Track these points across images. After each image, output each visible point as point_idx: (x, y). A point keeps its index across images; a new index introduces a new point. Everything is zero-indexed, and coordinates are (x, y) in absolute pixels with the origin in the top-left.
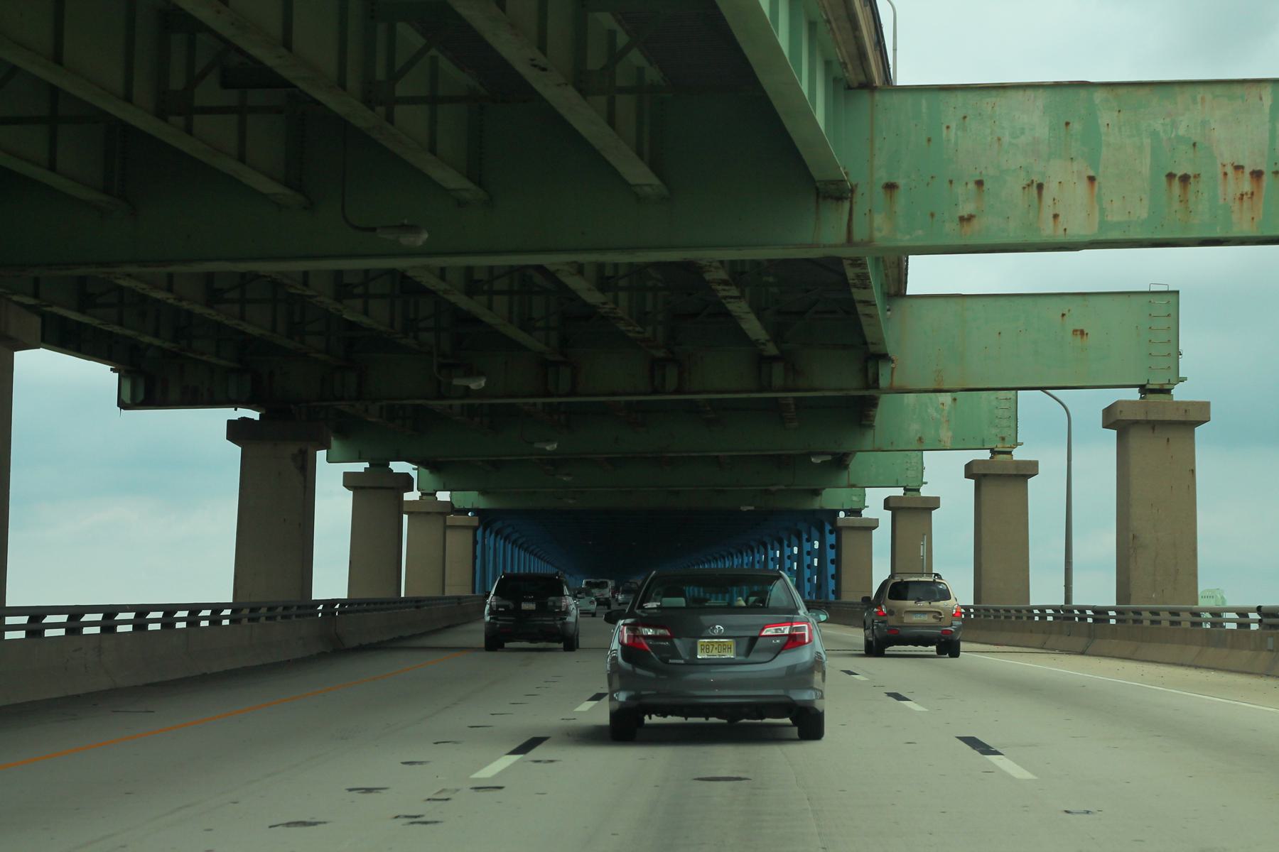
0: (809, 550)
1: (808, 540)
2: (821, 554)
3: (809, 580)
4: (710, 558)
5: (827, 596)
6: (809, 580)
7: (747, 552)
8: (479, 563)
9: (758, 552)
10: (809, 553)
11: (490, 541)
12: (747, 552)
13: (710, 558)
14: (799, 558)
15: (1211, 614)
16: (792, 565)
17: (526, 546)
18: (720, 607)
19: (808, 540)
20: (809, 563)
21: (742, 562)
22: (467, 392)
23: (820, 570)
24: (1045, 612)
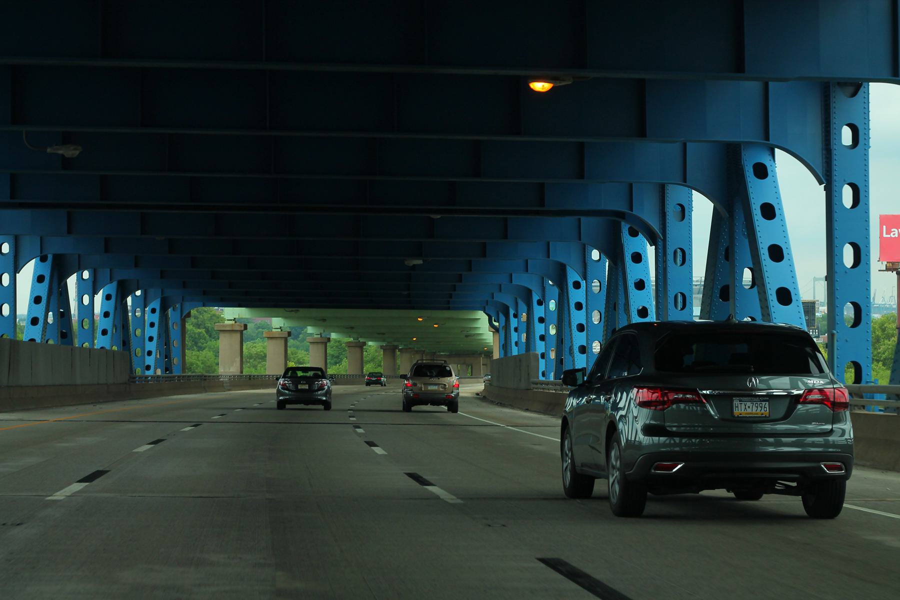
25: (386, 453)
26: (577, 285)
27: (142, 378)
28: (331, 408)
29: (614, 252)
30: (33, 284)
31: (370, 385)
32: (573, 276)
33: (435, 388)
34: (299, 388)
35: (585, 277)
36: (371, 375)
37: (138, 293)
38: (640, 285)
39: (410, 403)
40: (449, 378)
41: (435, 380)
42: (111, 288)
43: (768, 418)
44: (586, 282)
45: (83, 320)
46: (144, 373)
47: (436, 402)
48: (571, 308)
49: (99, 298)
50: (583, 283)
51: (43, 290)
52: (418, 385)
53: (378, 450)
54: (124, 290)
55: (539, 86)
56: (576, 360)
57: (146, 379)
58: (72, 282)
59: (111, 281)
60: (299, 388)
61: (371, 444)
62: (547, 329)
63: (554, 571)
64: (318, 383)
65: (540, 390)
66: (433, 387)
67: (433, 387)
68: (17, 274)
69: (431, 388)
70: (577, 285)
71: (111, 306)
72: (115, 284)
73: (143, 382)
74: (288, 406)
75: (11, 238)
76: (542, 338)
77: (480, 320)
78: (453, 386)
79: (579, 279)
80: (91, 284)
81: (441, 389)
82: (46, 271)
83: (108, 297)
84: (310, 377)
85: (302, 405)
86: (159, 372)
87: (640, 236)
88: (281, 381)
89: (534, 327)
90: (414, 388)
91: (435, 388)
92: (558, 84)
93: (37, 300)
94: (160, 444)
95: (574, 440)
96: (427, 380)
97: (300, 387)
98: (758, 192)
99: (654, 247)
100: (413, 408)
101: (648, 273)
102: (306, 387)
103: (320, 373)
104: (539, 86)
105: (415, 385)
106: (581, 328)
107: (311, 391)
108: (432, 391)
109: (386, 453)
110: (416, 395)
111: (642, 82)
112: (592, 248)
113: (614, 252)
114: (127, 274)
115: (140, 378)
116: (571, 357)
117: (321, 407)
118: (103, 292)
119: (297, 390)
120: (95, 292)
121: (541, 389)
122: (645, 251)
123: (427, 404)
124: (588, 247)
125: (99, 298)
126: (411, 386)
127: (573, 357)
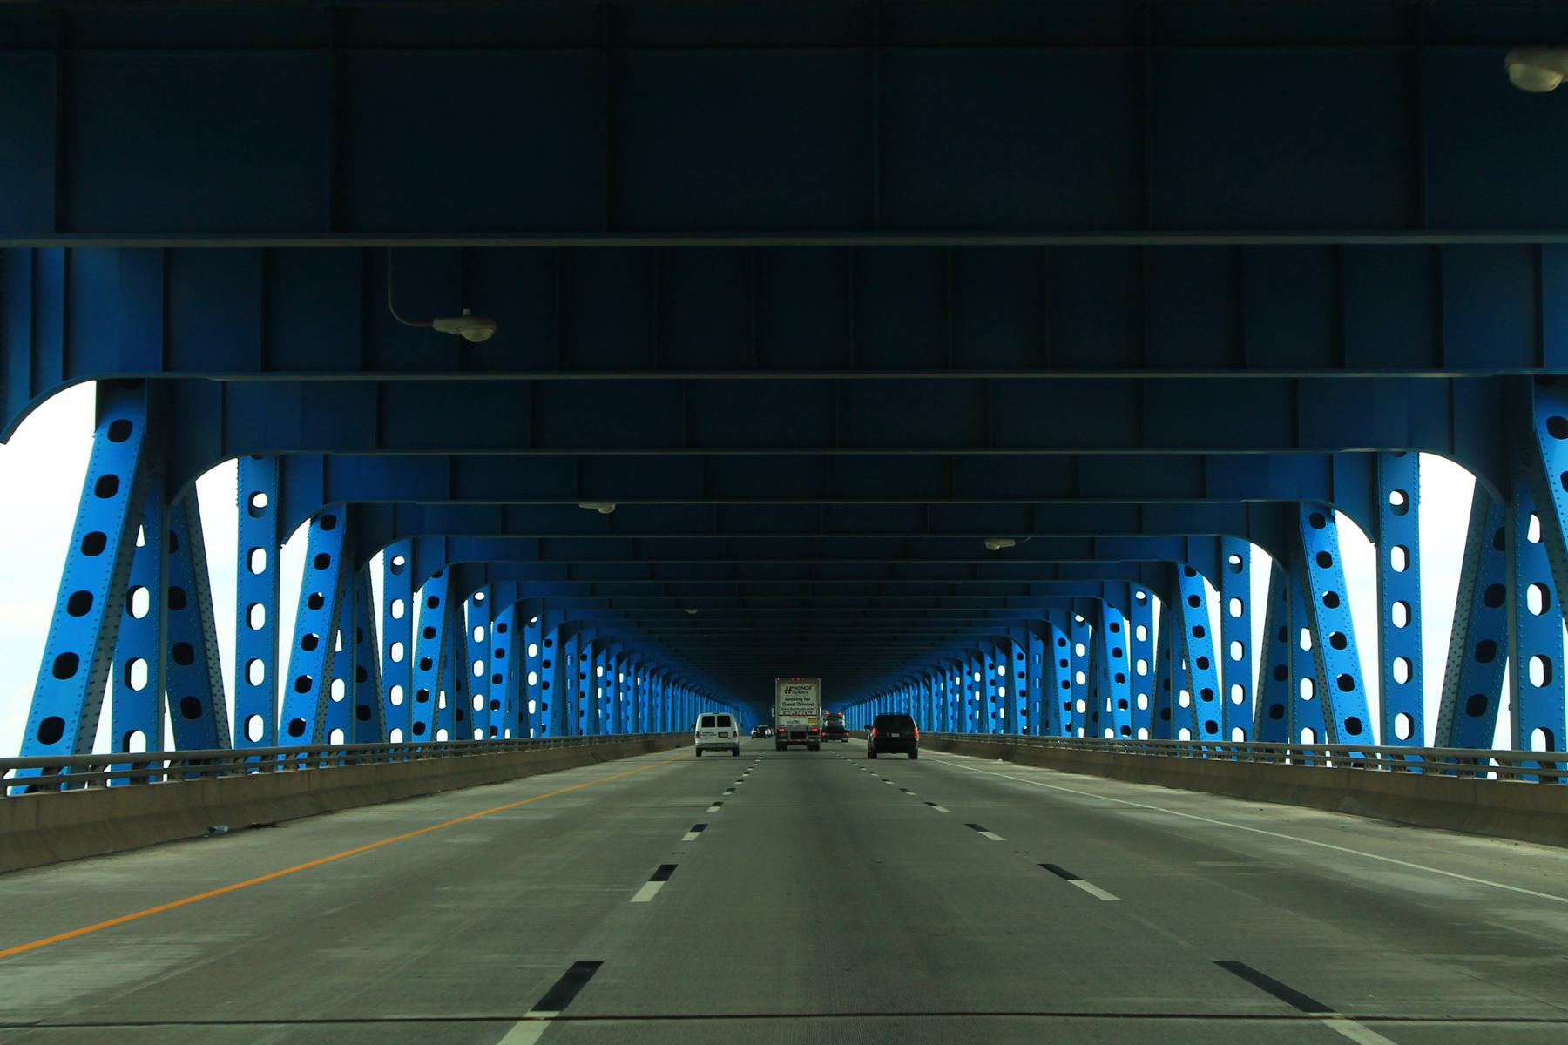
0: (970, 683)
1: (992, 667)
2: (1008, 681)
3: (994, 716)
4: (908, 680)
5: (1016, 732)
6: (971, 717)
7: (952, 672)
8: (859, 744)
9: (936, 683)
10: (992, 683)
11: (686, 695)
12: (913, 686)
13: (908, 680)
14: (982, 686)
15: (1222, 748)
16: (973, 696)
17: (701, 691)
18: (638, 699)
19: (992, 667)
20: (970, 698)
21: (919, 693)
22: (688, 615)
23: (1008, 702)
24: (1348, 755)
26: (1062, 643)
31: (826, 741)
32: (1059, 634)
35: (1069, 636)
37: (480, 596)
38: (1118, 653)
46: (540, 736)
50: (1068, 642)
54: (458, 593)
57: (413, 751)
58: (377, 564)
59: (486, 583)
62: (997, 691)
70: (1062, 643)
71: (437, 618)
73: (303, 767)
74: (789, 747)
76: (993, 699)
77: (602, 966)
79: (1063, 636)
82: (332, 544)
83: (432, 602)
87: (1198, 574)
89: (148, 979)
93: (314, 602)
95: (907, 762)
98: (1315, 542)
100: (879, 755)
106: (1066, 684)
111: (1536, 248)
115: (396, 750)
118: (424, 592)
122: (1123, 624)
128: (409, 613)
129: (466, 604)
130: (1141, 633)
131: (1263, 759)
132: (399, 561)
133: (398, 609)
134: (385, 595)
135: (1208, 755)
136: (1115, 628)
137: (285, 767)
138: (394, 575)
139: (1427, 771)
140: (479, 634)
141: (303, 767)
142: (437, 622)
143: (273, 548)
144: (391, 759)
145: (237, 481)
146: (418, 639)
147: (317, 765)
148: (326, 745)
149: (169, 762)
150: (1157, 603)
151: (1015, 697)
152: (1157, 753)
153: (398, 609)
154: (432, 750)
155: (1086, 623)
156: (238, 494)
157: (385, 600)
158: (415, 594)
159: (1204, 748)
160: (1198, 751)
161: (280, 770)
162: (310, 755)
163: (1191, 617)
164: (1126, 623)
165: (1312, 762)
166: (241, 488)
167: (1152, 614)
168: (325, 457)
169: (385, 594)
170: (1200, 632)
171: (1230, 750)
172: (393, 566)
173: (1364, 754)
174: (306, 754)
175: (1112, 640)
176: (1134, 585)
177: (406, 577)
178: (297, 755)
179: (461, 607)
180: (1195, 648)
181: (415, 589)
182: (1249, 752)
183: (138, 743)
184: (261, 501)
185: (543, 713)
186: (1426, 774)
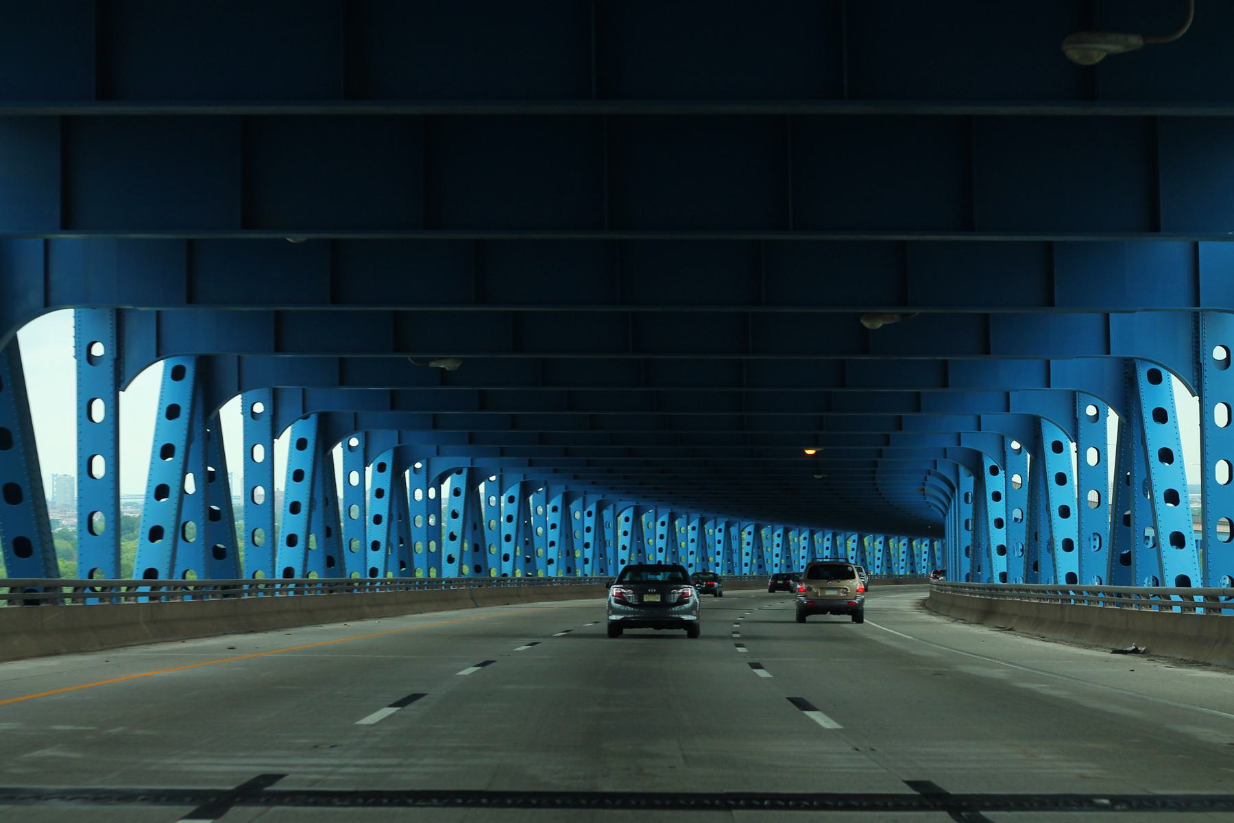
25: (771, 676)
27: (433, 582)
28: (699, 634)
29: (1034, 444)
30: (290, 452)
33: (834, 593)
34: (645, 600)
36: (776, 577)
38: (1061, 479)
39: (804, 613)
40: (851, 581)
41: (834, 583)
42: (307, 429)
43: (488, 551)
44: (1005, 473)
45: (350, 507)
47: (837, 611)
48: (1151, 459)
49: (283, 444)
51: (177, 433)
52: (814, 589)
53: (761, 673)
55: (810, 452)
56: (993, 561)
58: (338, 452)
60: (645, 600)
61: (757, 666)
63: (939, 784)
64: (676, 595)
65: (1008, 599)
66: (832, 591)
67: (832, 591)
68: (121, 393)
69: (829, 593)
71: (305, 461)
72: (313, 419)
74: (626, 631)
75: (266, 392)
78: (857, 591)
80: (360, 452)
81: (842, 595)
82: (183, 393)
83: (301, 444)
84: (663, 582)
85: (651, 629)
86: (390, 575)
88: (614, 590)
90: (808, 593)
91: (834, 593)
92: (819, 449)
93: (298, 476)
94: (481, 662)
96: (824, 583)
97: (647, 598)
99: (1197, 398)
100: (809, 618)
101: (1070, 467)
102: (657, 598)
103: (680, 575)
104: (810, 452)
105: (809, 589)
107: (665, 605)
108: (829, 596)
109: (771, 676)
110: (812, 602)
112: (1011, 440)
113: (1034, 444)
114: (335, 399)
116: (988, 559)
117: (683, 632)
118: (293, 432)
119: (642, 605)
120: (275, 433)
121: (1044, 599)
123: (825, 613)
124: (1007, 439)
125: (283, 444)
126: (805, 591)
127: (1053, 555)
128: (269, 460)
129: (407, 473)
130: (1092, 457)
131: (975, 594)
132: (259, 408)
133: (355, 478)
134: (344, 469)
135: (1075, 601)
136: (1058, 447)
137: (358, 590)
138: (350, 453)
139: (1162, 609)
140: (419, 495)
141: (291, 594)
142: (460, 507)
143: (111, 396)
144: (306, 592)
145: (73, 329)
146: (371, 498)
147: (302, 593)
148: (488, 577)
149: (280, 585)
150: (1112, 420)
151: (987, 528)
152: (945, 590)
153: (355, 478)
154: (529, 582)
155: (1023, 449)
156: (242, 403)
157: (344, 473)
158: (367, 468)
159: (1085, 594)
160: (1079, 596)
161: (246, 596)
162: (297, 585)
163: (1156, 436)
164: (1073, 446)
165: (1157, 607)
166: (77, 337)
167: (1105, 433)
168: (158, 313)
169: (344, 469)
170: (1167, 456)
171: (1046, 593)
172: (253, 415)
173: (1181, 596)
174: (321, 584)
175: (1054, 463)
176: (1081, 398)
177: (360, 455)
178: (136, 588)
179: (402, 476)
180: (1162, 476)
181: (366, 464)
182: (1084, 595)
183: (433, 574)
184: (98, 350)
185: (586, 565)
186: (1210, 614)
